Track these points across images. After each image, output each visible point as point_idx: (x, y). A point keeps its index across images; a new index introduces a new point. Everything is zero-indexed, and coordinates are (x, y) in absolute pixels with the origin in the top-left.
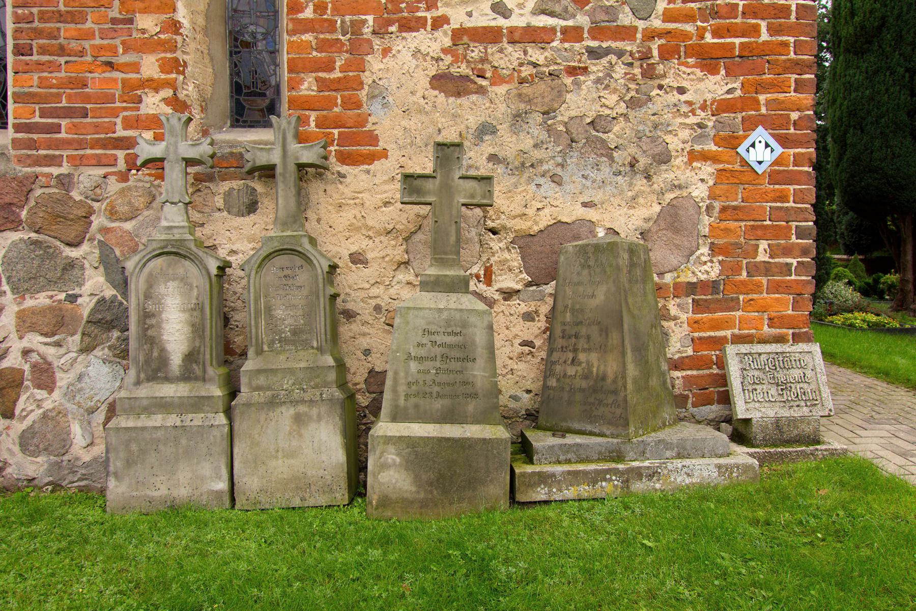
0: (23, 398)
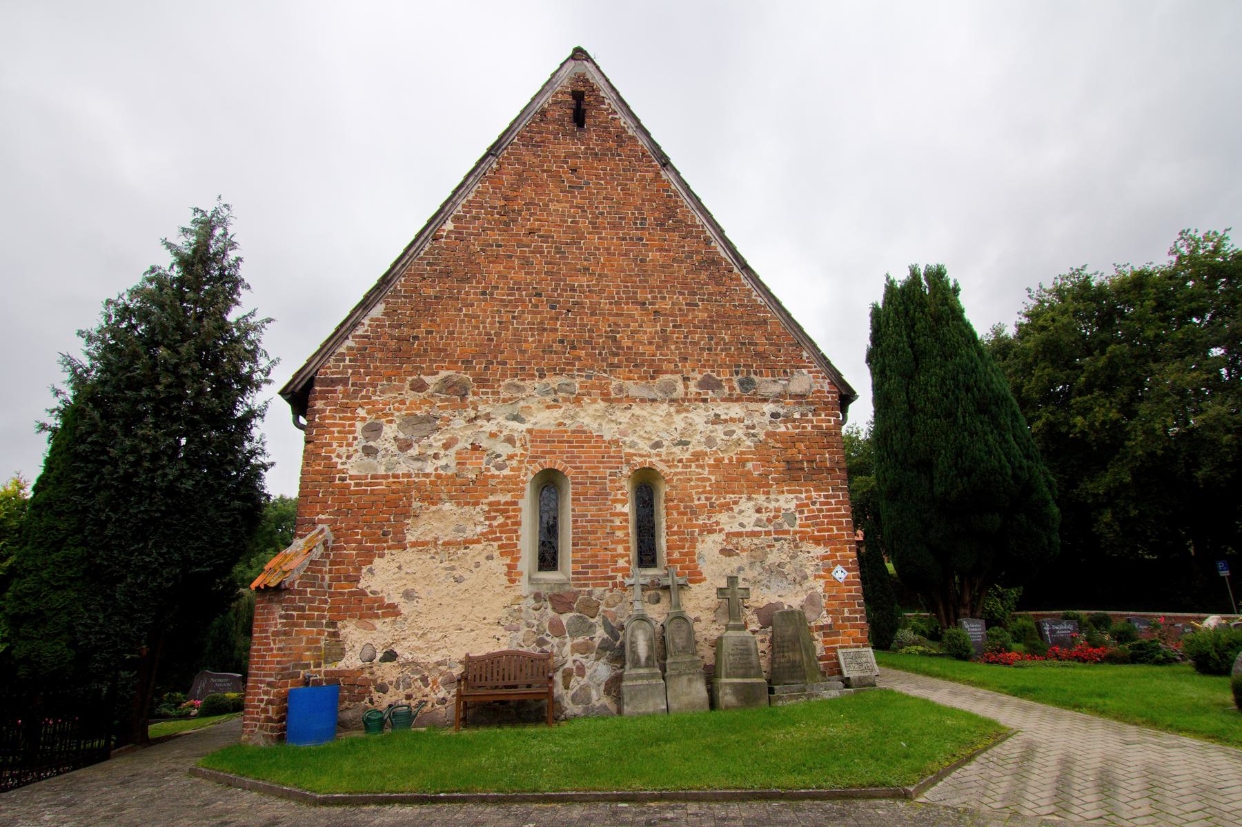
0: (572, 680)
